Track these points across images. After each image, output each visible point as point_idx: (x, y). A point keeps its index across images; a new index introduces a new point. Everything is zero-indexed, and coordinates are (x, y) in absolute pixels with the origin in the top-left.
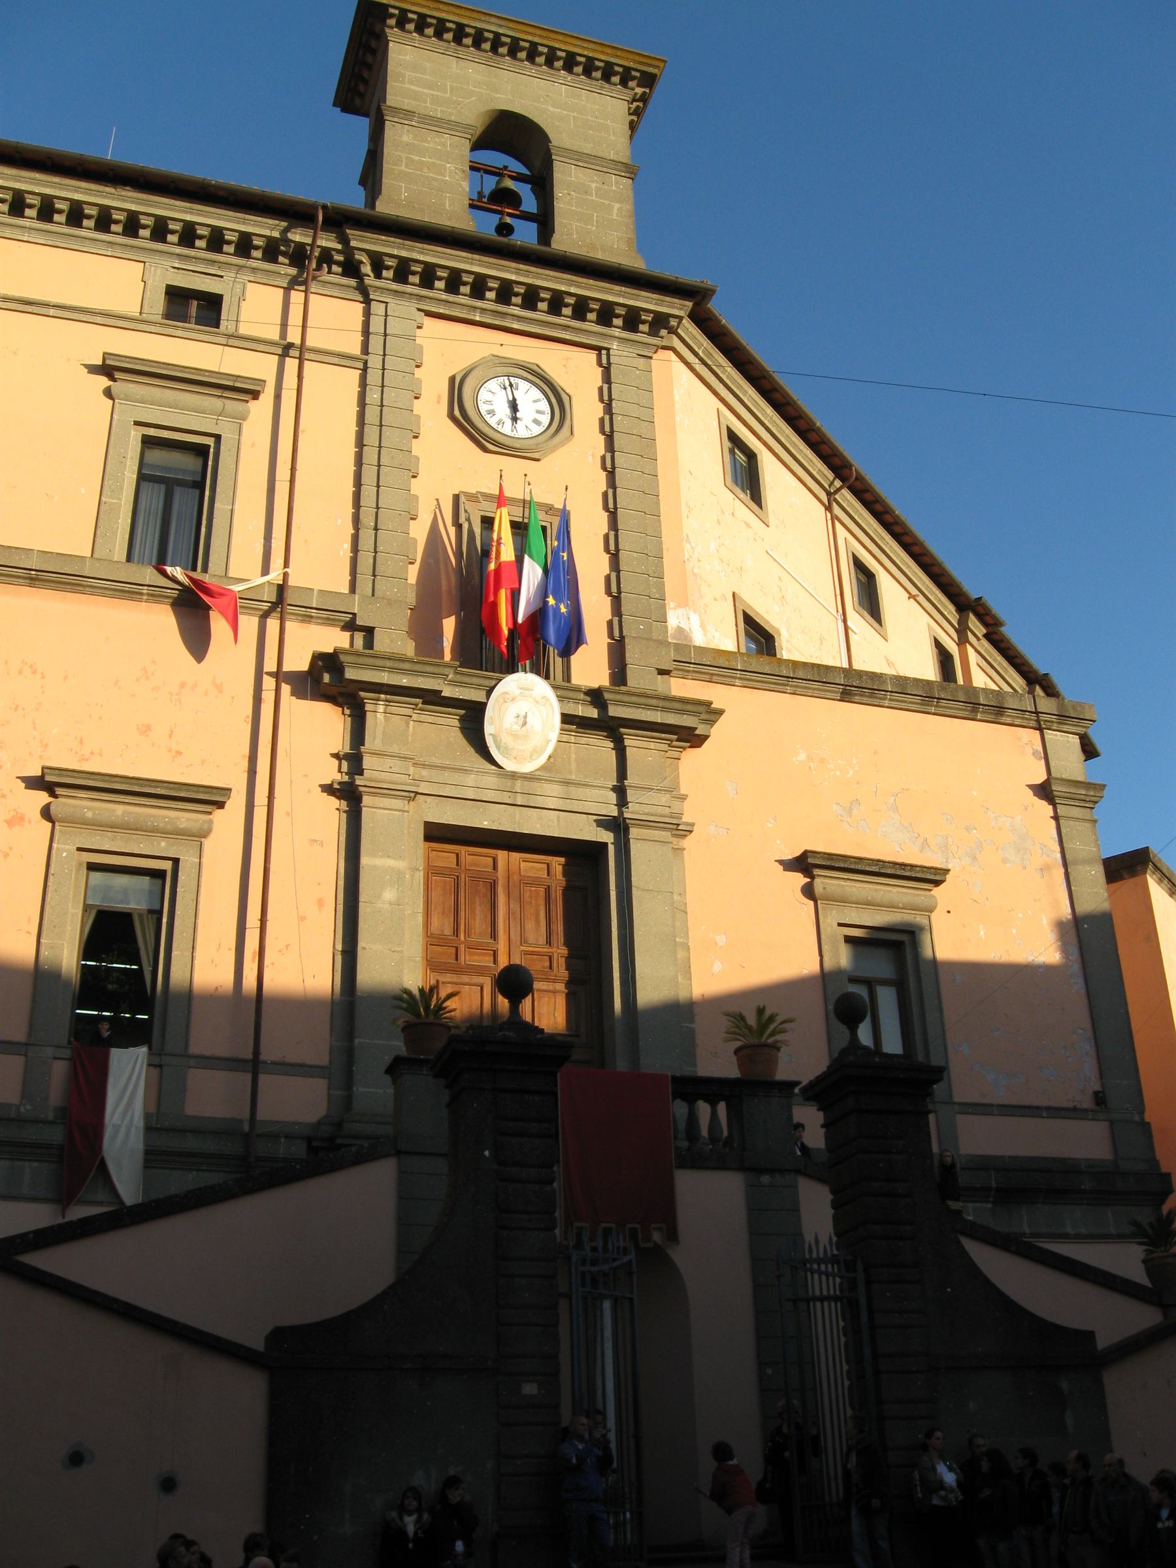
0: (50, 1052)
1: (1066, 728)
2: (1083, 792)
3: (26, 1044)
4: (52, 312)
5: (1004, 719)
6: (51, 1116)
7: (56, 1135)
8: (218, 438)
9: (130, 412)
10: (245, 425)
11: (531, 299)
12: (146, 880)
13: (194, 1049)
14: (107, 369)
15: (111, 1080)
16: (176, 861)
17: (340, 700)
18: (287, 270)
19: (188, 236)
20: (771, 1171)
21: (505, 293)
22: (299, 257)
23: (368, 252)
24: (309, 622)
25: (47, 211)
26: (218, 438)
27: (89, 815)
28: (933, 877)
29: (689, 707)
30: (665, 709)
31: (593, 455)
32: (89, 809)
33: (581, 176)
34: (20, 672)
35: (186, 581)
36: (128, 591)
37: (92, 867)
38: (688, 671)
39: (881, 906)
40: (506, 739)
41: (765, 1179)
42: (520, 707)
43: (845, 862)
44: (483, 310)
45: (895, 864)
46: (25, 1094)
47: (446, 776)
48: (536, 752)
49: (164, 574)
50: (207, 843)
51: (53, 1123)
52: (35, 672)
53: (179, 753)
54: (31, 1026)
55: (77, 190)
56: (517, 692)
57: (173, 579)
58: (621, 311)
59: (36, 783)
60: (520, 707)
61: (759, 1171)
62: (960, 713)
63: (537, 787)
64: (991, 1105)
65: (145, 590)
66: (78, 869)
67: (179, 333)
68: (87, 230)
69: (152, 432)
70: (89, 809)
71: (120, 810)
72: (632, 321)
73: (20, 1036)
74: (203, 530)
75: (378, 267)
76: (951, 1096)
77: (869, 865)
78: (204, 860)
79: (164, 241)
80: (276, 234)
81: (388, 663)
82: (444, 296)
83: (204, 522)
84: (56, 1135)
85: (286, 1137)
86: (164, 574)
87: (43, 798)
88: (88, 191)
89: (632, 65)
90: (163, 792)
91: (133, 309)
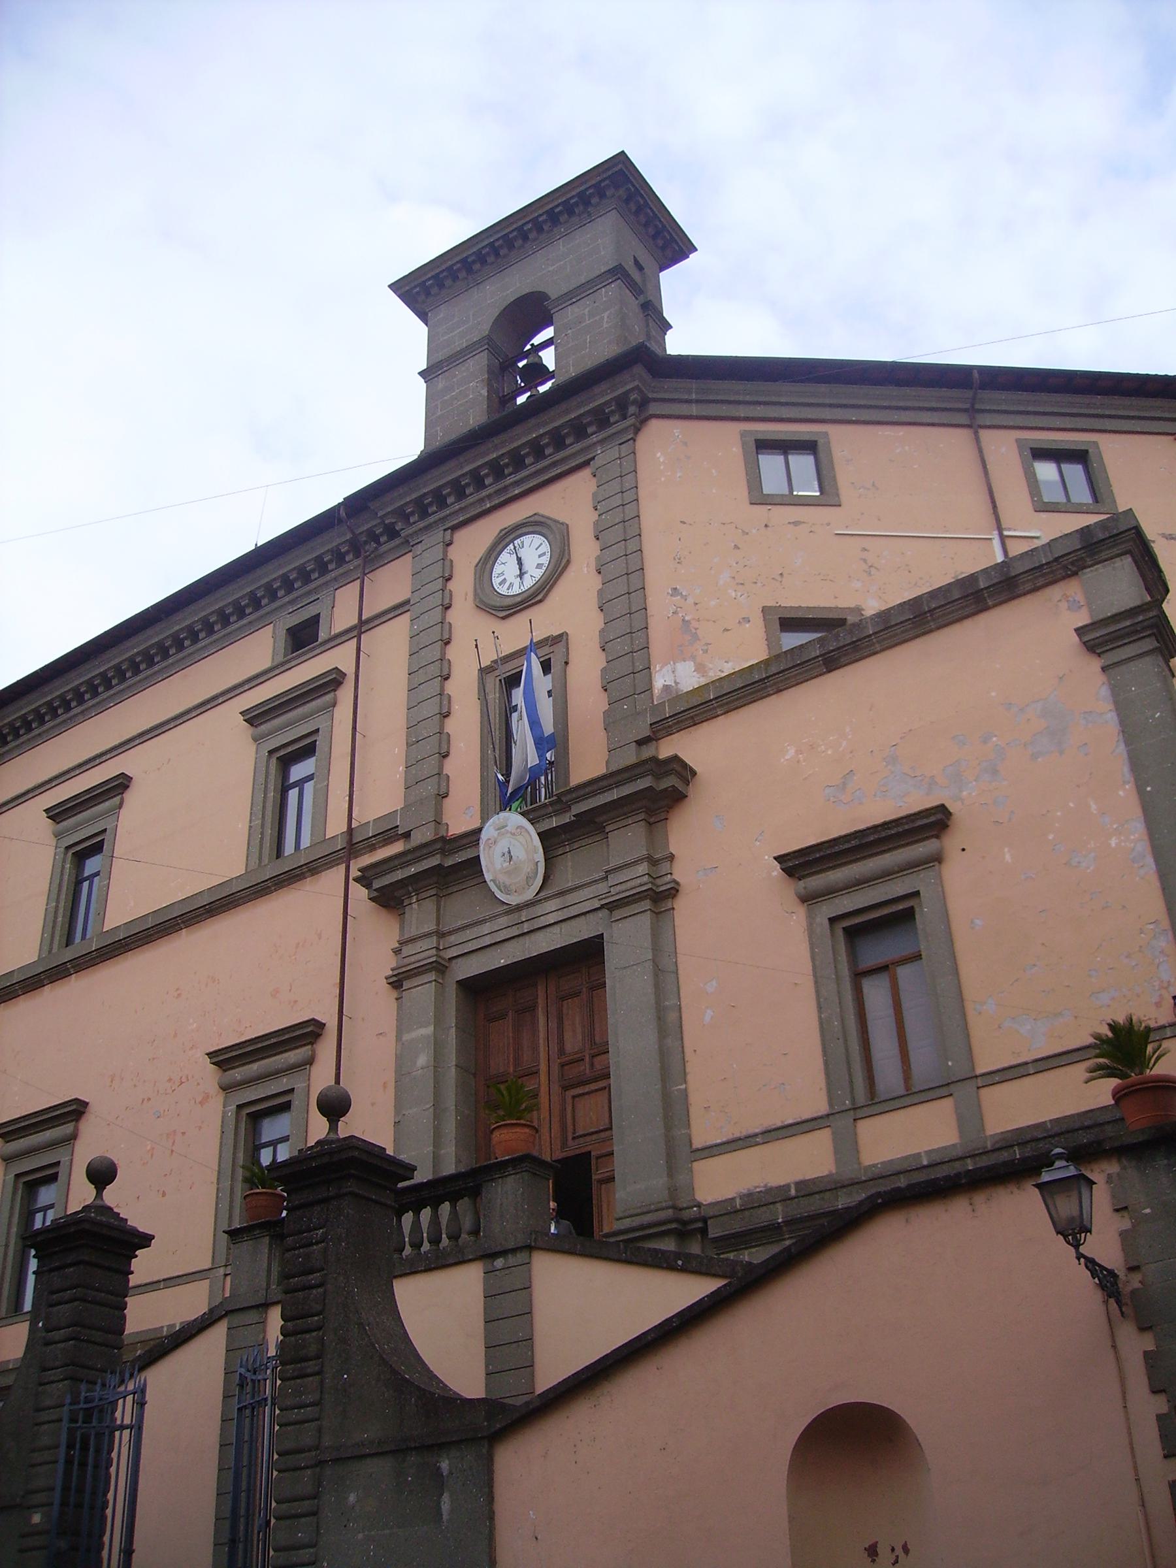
1: (1104, 555)
2: (1128, 623)
5: (1021, 589)
11: (518, 462)
17: (392, 903)
18: (354, 563)
20: (503, 1253)
21: (497, 471)
22: (356, 548)
23: (392, 512)
24: (375, 849)
29: (637, 771)
30: (618, 784)
31: (588, 566)
33: (576, 310)
38: (670, 727)
40: (502, 878)
41: (499, 1263)
42: (503, 845)
43: (820, 850)
44: (489, 497)
45: (875, 827)
47: (469, 934)
48: (529, 879)
56: (495, 834)
60: (503, 845)
61: (492, 1256)
62: (967, 611)
63: (539, 910)
64: (1026, 1063)
71: (255, 1067)
72: (602, 419)
75: (406, 517)
77: (849, 842)
80: (349, 536)
81: (397, 862)
89: (520, 223)
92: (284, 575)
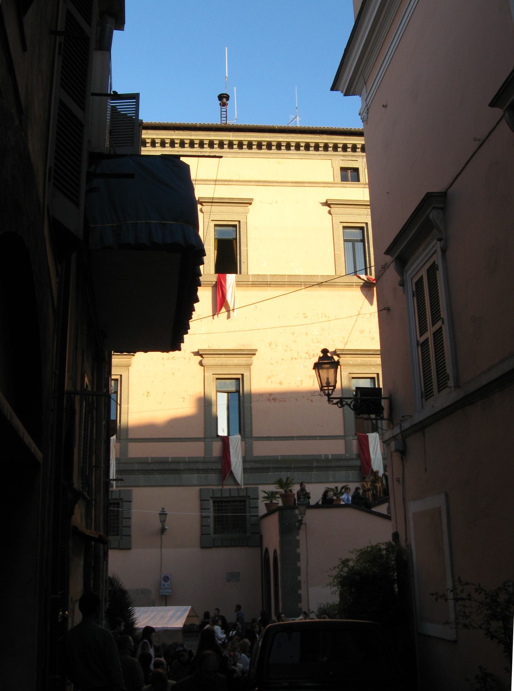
0: (351, 438)
3: (344, 436)
4: (306, 185)
6: (355, 457)
7: (219, 466)
8: (239, 221)
9: (338, 219)
10: (248, 215)
11: (269, 146)
12: (234, 381)
13: (255, 434)
14: (327, 204)
15: (231, 448)
16: (243, 375)
19: (345, 148)
25: (298, 147)
26: (239, 221)
27: (351, 362)
28: (252, 353)
32: (351, 360)
34: (322, 317)
35: (366, 279)
36: (350, 285)
37: (217, 379)
39: (232, 367)
46: (346, 451)
49: (359, 278)
50: (251, 367)
51: (356, 459)
52: (326, 316)
53: (373, 338)
54: (345, 431)
55: (307, 138)
57: (363, 280)
58: (265, 143)
59: (197, 354)
65: (354, 284)
66: (213, 380)
67: (348, 185)
68: (312, 151)
69: (345, 225)
70: (351, 360)
73: (341, 433)
74: (367, 258)
76: (252, 434)
78: (252, 374)
79: (165, 147)
82: (342, 153)
83: (367, 255)
84: (358, 463)
85: (138, 463)
86: (359, 278)
87: (199, 358)
88: (311, 138)
90: (245, 353)
91: (332, 180)
92: (327, 143)
